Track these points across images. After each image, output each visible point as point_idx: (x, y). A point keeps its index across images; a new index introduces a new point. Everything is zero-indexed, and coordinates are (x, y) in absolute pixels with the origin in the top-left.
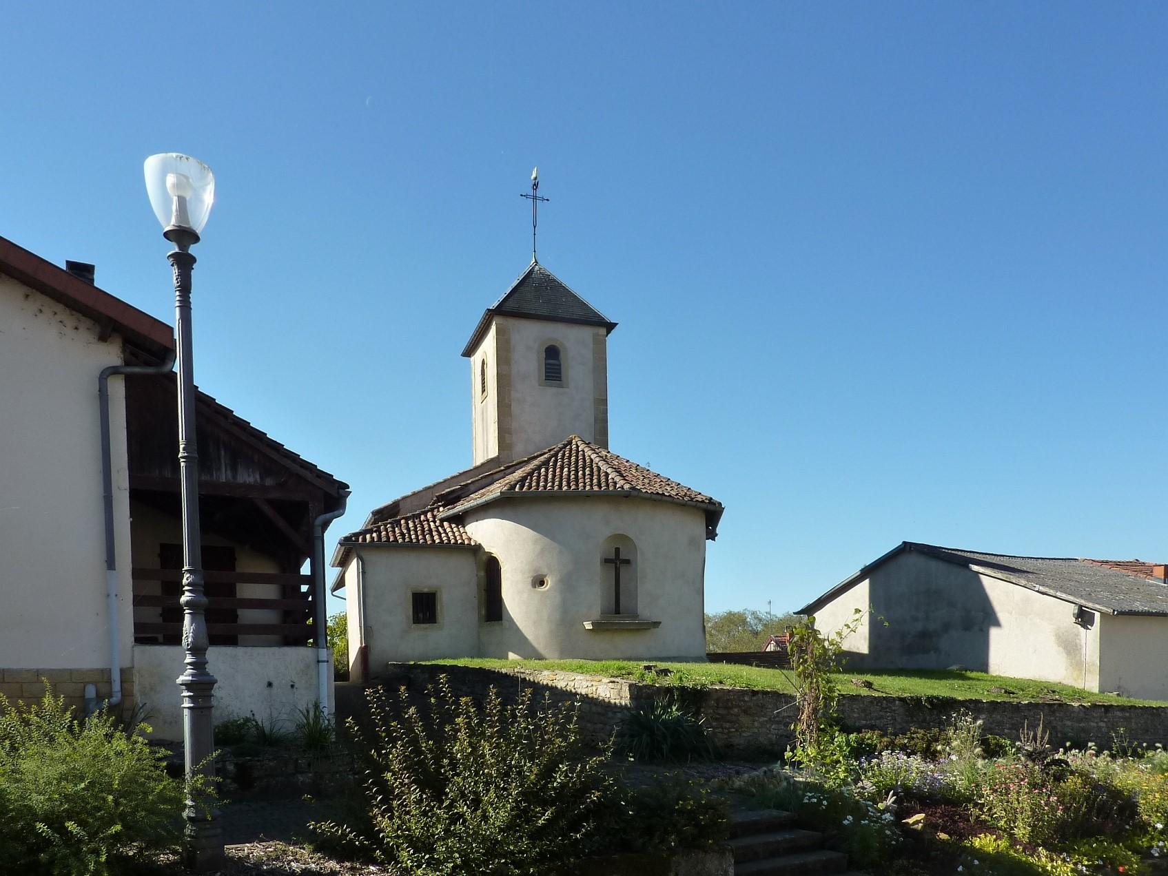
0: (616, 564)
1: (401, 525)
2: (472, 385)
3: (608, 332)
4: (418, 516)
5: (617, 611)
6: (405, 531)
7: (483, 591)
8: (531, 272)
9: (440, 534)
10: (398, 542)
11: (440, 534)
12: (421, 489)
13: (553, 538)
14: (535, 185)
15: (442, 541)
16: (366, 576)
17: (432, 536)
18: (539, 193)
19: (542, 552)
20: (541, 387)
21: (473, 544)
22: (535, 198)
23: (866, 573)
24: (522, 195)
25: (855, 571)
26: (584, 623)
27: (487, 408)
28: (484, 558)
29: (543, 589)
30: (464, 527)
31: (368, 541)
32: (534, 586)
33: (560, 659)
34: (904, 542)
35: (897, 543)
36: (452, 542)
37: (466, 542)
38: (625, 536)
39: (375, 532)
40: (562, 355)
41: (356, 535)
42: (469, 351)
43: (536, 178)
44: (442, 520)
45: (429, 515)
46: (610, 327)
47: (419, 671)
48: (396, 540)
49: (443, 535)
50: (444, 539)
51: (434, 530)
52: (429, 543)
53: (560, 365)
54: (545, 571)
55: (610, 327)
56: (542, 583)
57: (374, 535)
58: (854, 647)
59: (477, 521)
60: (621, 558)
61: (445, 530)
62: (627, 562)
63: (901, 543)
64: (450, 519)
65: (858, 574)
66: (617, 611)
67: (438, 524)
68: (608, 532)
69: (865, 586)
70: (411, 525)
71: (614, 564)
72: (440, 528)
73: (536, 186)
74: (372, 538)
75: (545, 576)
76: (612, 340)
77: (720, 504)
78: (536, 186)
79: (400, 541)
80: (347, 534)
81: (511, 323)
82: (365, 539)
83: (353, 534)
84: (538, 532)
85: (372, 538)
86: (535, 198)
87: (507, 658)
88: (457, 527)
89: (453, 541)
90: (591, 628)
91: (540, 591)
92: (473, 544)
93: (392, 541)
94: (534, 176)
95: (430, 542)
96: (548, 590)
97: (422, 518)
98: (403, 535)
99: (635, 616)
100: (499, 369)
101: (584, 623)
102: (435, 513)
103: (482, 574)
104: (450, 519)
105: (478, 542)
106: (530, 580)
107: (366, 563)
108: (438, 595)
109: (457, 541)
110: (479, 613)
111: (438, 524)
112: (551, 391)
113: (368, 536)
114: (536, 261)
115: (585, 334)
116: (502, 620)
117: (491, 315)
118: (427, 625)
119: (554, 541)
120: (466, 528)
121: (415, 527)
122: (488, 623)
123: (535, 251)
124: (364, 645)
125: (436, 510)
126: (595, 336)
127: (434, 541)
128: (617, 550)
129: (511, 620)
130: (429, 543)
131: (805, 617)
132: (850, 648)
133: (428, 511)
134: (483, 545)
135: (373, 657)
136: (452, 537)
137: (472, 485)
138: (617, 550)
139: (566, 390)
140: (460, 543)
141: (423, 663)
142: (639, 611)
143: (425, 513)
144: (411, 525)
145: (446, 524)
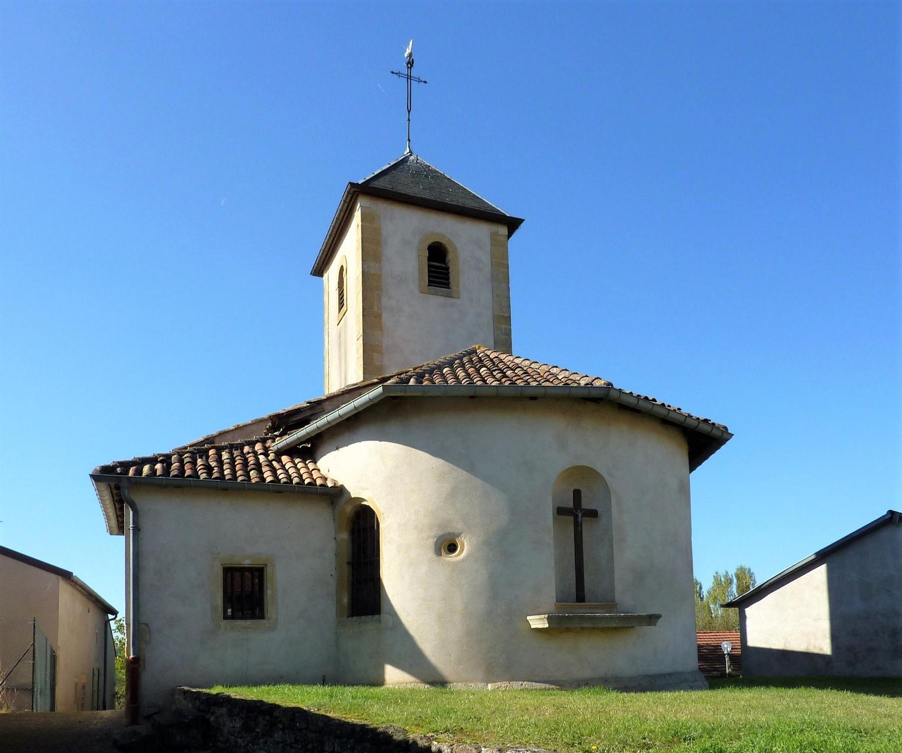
0: (576, 517)
1: (208, 457)
2: (323, 308)
3: (510, 234)
4: (241, 447)
5: (580, 597)
6: (213, 464)
7: (346, 565)
8: (405, 160)
9: (274, 471)
10: (199, 477)
11: (274, 471)
12: (250, 422)
13: (471, 468)
14: (409, 63)
15: (277, 480)
16: (141, 536)
17: (261, 473)
18: (415, 72)
19: (453, 494)
20: (421, 295)
21: (330, 484)
22: (409, 77)
23: (822, 557)
24: (393, 72)
25: (808, 555)
26: (528, 618)
27: (345, 332)
28: (349, 509)
29: (454, 558)
30: (315, 463)
31: (144, 475)
32: (438, 552)
33: (488, 682)
34: (891, 512)
35: (878, 513)
36: (294, 482)
37: (319, 482)
38: (591, 468)
39: (162, 462)
40: (450, 256)
41: (126, 465)
42: (319, 270)
43: (410, 55)
44: (279, 453)
45: (258, 447)
46: (513, 224)
47: (224, 710)
48: (195, 475)
49: (279, 472)
50: (280, 477)
51: (263, 464)
52: (253, 481)
53: (448, 269)
54: (458, 526)
55: (513, 224)
56: (452, 548)
57: (158, 466)
58: (815, 648)
59: (337, 449)
60: (582, 508)
61: (283, 467)
62: (593, 514)
63: (885, 513)
64: (292, 451)
65: (813, 557)
66: (580, 597)
67: (272, 456)
68: (562, 462)
69: (820, 573)
70: (225, 456)
71: (571, 518)
72: (274, 463)
73: (410, 64)
74: (153, 471)
75: (459, 535)
76: (516, 242)
77: (726, 428)
78: (410, 64)
79: (203, 476)
80: (109, 462)
81: (385, 210)
82: (139, 472)
83: (118, 463)
84: (446, 461)
85: (153, 471)
86: (409, 77)
87: (379, 682)
88: (304, 461)
89: (296, 480)
90: (547, 626)
91: (449, 563)
92: (330, 484)
93: (189, 476)
94: (408, 51)
95: (257, 480)
96: (463, 560)
97: (246, 449)
98: (209, 469)
99: (611, 605)
100: (365, 266)
101: (528, 618)
102: (267, 445)
103: (345, 536)
104: (292, 451)
105: (340, 483)
106: (431, 542)
107: (141, 513)
108: (268, 571)
109: (304, 481)
110: (339, 602)
111: (272, 456)
112: (436, 301)
113: (146, 469)
114: (410, 151)
115: (482, 231)
116: (379, 613)
117: (357, 191)
118: (249, 623)
119: (476, 476)
120: (318, 464)
121: (232, 460)
122: (355, 618)
123: (409, 140)
124: (131, 656)
125: (270, 441)
126: (493, 236)
127: (263, 479)
128: (577, 494)
129: (394, 614)
130: (253, 481)
131: (733, 612)
132: (821, 649)
133: (257, 442)
134: (347, 487)
135: (147, 678)
136: (295, 475)
137: (327, 403)
138: (577, 494)
139: (455, 300)
140: (309, 484)
141: (237, 693)
142: (618, 597)
143: (252, 444)
144: (225, 456)
145: (285, 459)
